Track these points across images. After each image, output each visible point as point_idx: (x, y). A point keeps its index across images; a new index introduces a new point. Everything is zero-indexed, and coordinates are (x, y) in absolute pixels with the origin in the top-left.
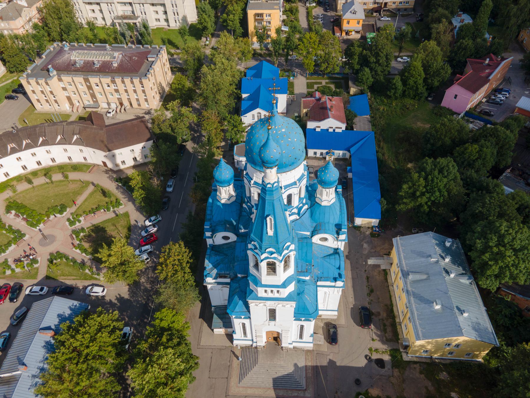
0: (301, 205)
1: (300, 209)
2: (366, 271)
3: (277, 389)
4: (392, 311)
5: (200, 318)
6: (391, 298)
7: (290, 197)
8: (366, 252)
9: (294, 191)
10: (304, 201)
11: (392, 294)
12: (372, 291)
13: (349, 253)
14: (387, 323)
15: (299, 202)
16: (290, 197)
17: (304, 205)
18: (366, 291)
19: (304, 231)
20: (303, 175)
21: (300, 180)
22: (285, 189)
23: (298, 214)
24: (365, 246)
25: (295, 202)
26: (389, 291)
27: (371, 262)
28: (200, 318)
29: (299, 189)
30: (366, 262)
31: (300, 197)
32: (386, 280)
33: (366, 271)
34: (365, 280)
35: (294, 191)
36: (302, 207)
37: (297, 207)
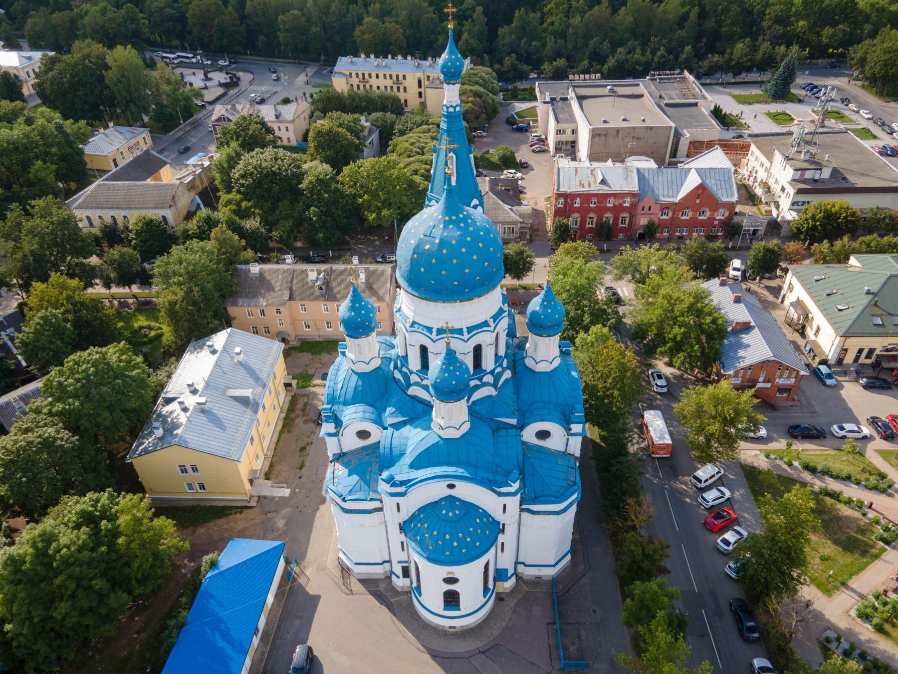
0: (499, 369)
1: (497, 377)
2: (300, 478)
3: (450, 602)
4: (284, 426)
5: (316, 599)
6: (278, 441)
7: (478, 350)
8: (286, 511)
9: (485, 338)
10: (505, 364)
11: (273, 446)
12: (303, 449)
13: (318, 509)
14: (299, 412)
15: (496, 363)
16: (478, 350)
17: (504, 370)
18: (311, 450)
19: (507, 417)
20: (501, 311)
21: (496, 317)
22: (469, 332)
23: (495, 385)
24: (281, 524)
25: (488, 363)
26: (275, 449)
27: (286, 492)
28: (316, 599)
29: (494, 335)
30: (293, 493)
31: (496, 355)
32: (272, 465)
33: (300, 478)
34: (307, 464)
35: (485, 338)
36: (500, 375)
37: (492, 372)
